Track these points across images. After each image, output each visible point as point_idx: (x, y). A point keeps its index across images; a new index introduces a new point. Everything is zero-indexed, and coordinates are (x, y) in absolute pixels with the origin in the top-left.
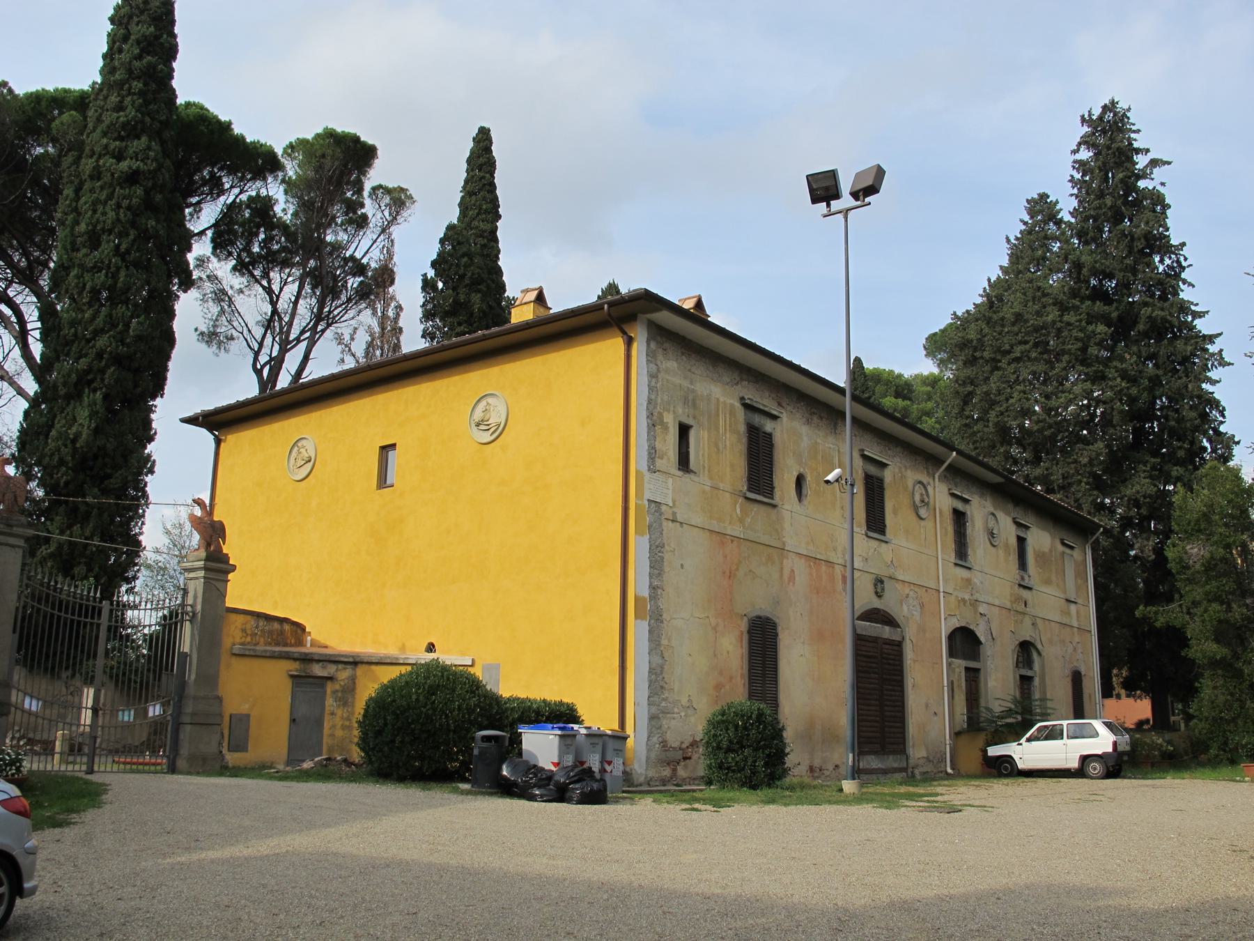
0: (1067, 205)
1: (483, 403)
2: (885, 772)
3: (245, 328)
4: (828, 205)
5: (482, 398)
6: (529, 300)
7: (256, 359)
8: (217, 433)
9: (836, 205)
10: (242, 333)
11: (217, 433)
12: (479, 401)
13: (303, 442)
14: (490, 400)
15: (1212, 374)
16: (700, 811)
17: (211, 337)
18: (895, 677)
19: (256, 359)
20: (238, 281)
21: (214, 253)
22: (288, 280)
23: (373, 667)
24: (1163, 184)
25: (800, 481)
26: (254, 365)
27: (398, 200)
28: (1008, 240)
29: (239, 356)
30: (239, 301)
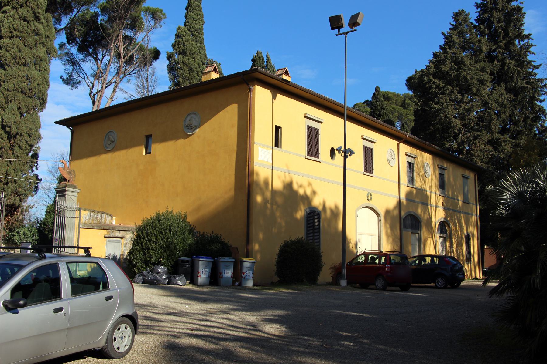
0: (473, 15)
1: (189, 118)
2: (250, 315)
3: (86, 76)
4: (339, 31)
5: (189, 114)
6: (210, 67)
7: (91, 92)
8: (72, 128)
9: (342, 31)
10: (84, 79)
11: (72, 128)
12: (188, 116)
13: (112, 133)
14: (193, 115)
15: (541, 98)
16: (187, 329)
17: (68, 81)
18: (224, 294)
19: (91, 92)
20: (80, 56)
21: (68, 42)
22: (107, 54)
23: (271, 149)
24: (521, 3)
25: (60, 309)
26: (90, 94)
27: (155, 15)
28: (443, 33)
29: (83, 90)
30: (82, 64)
